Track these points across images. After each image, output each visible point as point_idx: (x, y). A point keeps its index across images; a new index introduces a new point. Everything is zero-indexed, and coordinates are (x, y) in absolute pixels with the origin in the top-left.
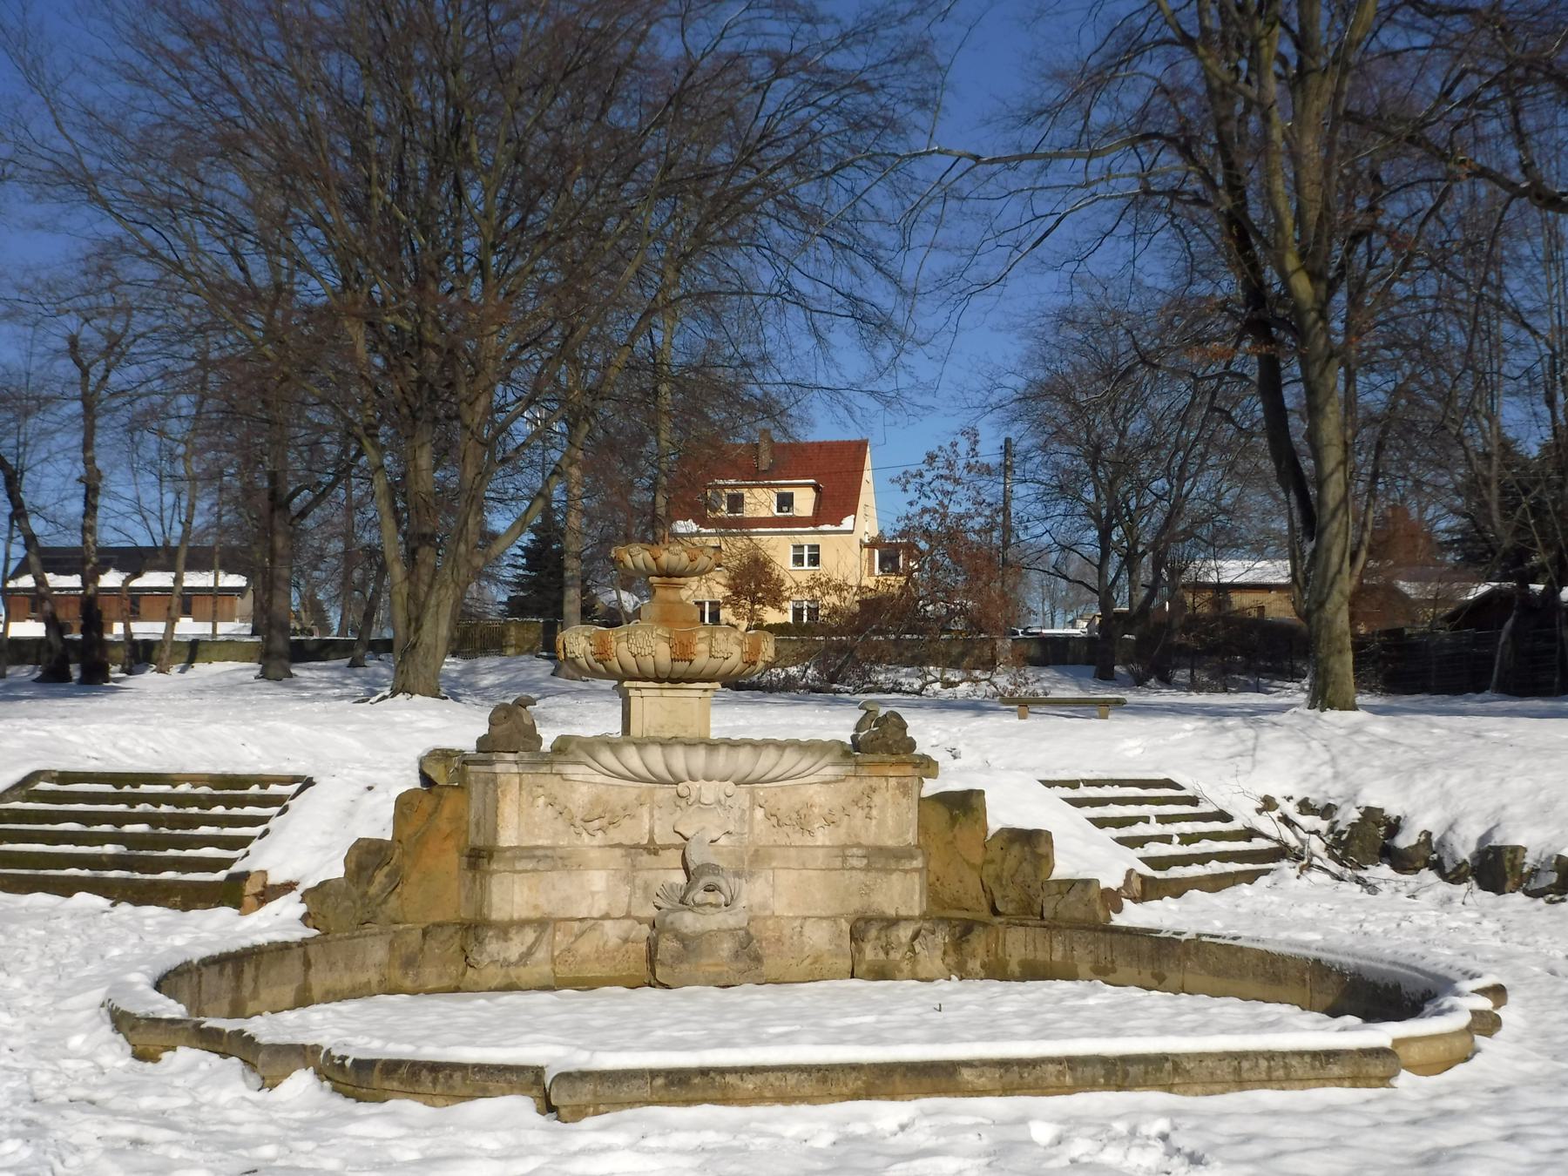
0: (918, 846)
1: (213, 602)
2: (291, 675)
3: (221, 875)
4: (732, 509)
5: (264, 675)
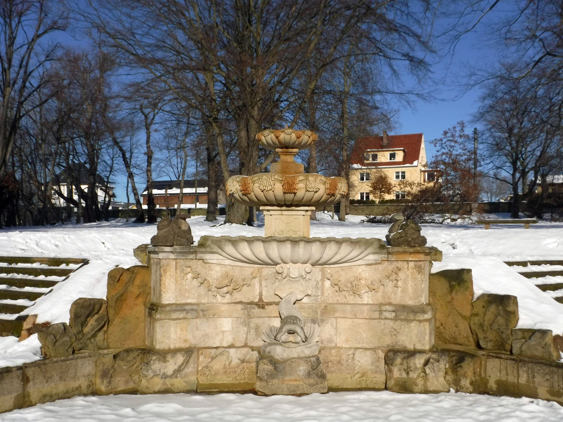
0: (428, 304)
1: (196, 197)
2: (216, 219)
3: (13, 317)
4: (373, 159)
5: (207, 219)
